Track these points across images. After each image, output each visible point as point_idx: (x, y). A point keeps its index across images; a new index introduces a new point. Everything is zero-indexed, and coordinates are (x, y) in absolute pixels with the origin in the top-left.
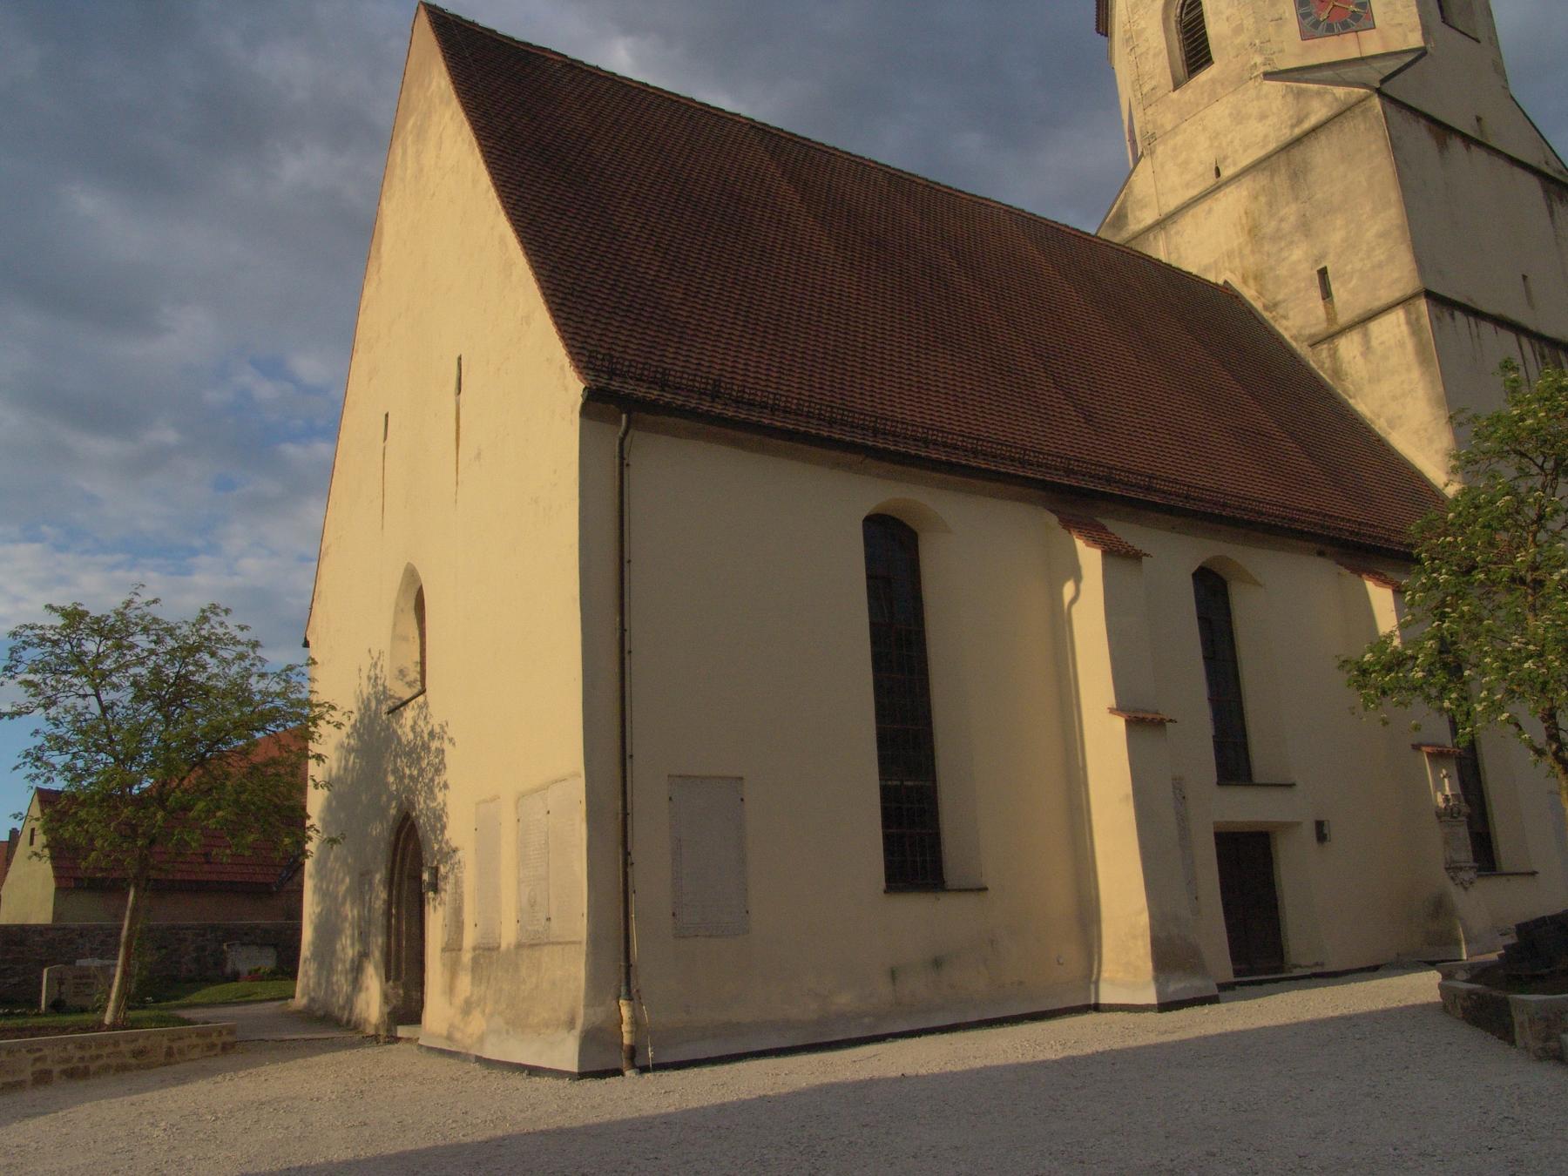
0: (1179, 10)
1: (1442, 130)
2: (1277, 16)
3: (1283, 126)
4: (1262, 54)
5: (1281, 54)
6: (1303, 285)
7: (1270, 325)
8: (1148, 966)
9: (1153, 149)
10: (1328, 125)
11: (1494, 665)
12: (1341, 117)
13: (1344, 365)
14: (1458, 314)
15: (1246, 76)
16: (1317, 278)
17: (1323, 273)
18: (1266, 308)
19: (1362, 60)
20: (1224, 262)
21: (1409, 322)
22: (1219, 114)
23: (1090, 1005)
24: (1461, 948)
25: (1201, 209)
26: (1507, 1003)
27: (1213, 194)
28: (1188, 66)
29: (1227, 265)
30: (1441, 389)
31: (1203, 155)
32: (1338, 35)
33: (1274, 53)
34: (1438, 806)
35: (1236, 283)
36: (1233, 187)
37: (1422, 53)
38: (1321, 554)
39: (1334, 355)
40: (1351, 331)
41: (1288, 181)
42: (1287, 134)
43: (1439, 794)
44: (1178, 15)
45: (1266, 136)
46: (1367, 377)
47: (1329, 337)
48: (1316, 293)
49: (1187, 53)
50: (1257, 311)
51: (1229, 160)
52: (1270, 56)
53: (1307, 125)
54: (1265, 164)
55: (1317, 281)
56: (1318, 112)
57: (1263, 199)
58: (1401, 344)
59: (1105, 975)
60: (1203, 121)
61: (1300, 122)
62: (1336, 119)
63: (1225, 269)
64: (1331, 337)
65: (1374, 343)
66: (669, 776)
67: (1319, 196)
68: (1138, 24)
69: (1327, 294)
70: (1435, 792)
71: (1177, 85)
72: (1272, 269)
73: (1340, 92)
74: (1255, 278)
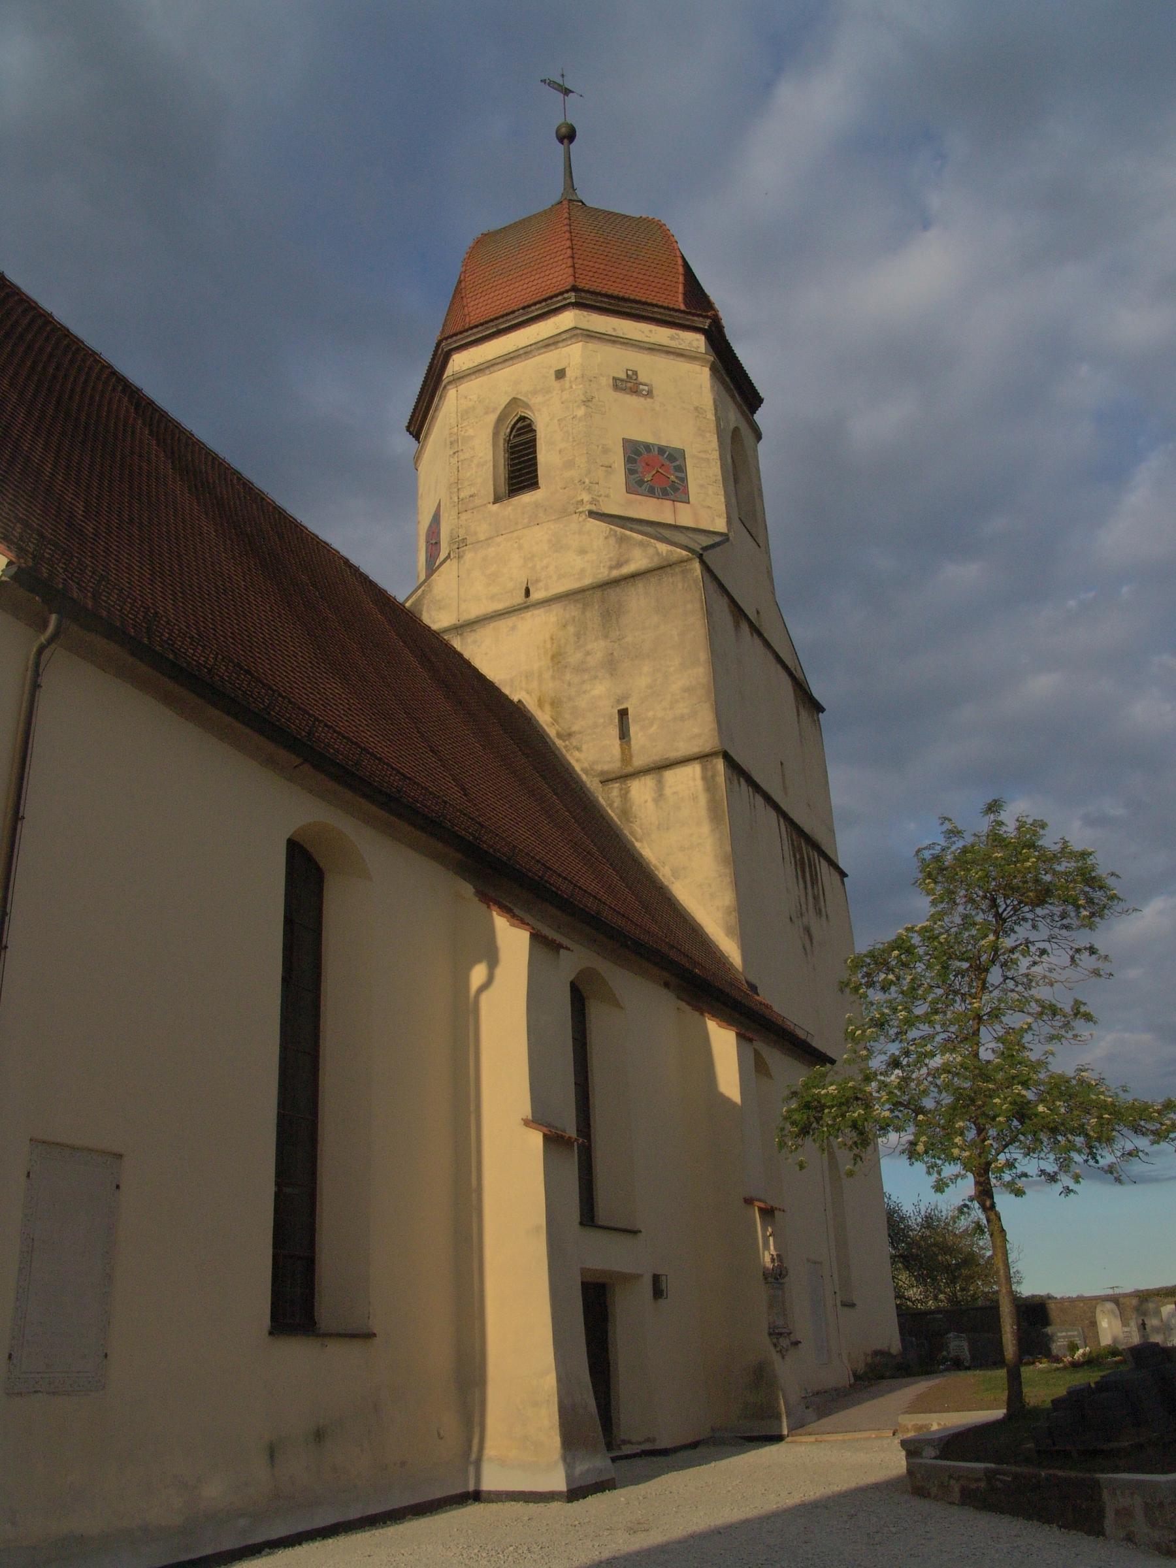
0: (509, 430)
1: (738, 611)
2: (607, 464)
3: (602, 565)
4: (590, 493)
5: (606, 499)
6: (602, 720)
7: (561, 753)
8: (554, 1441)
9: (461, 553)
10: (648, 575)
11: (1004, 1107)
12: (661, 571)
13: (634, 808)
14: (742, 781)
15: (571, 509)
16: (617, 716)
17: (623, 713)
18: (559, 735)
19: (676, 527)
20: (521, 681)
21: (704, 778)
22: (538, 537)
23: (468, 1493)
24: (781, 1422)
25: (504, 624)
26: (1097, 1484)
27: (519, 612)
28: (510, 485)
29: (524, 684)
30: (729, 848)
31: (514, 574)
32: (658, 498)
33: (600, 496)
34: (764, 1267)
35: (531, 704)
36: (542, 610)
37: (725, 538)
38: (667, 985)
39: (625, 795)
40: (644, 775)
41: (600, 619)
42: (604, 574)
43: (766, 1253)
44: (507, 434)
45: (583, 570)
46: (657, 823)
47: (621, 777)
48: (615, 732)
49: (510, 472)
50: (550, 738)
51: (541, 584)
52: (597, 498)
53: (627, 570)
54: (580, 596)
55: (617, 720)
56: (639, 561)
57: (571, 629)
58: (695, 798)
59: (490, 1451)
60: (520, 539)
61: (619, 565)
62: (655, 572)
63: (521, 688)
64: (625, 777)
65: (668, 791)
66: (31, 1140)
67: (629, 639)
68: (466, 430)
69: (624, 734)
70: (764, 1251)
71: (497, 500)
72: (570, 698)
73: (663, 548)
74: (552, 704)
